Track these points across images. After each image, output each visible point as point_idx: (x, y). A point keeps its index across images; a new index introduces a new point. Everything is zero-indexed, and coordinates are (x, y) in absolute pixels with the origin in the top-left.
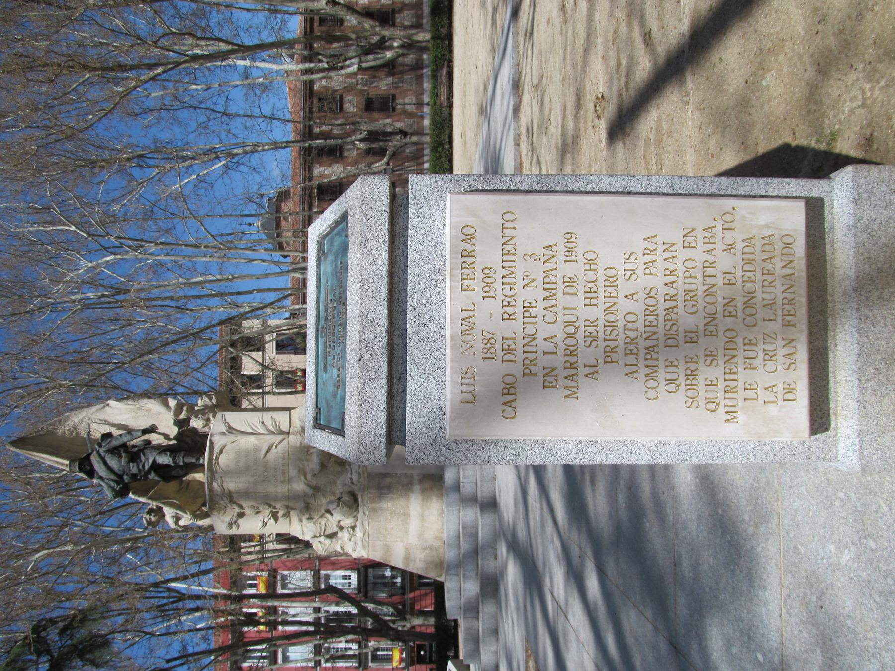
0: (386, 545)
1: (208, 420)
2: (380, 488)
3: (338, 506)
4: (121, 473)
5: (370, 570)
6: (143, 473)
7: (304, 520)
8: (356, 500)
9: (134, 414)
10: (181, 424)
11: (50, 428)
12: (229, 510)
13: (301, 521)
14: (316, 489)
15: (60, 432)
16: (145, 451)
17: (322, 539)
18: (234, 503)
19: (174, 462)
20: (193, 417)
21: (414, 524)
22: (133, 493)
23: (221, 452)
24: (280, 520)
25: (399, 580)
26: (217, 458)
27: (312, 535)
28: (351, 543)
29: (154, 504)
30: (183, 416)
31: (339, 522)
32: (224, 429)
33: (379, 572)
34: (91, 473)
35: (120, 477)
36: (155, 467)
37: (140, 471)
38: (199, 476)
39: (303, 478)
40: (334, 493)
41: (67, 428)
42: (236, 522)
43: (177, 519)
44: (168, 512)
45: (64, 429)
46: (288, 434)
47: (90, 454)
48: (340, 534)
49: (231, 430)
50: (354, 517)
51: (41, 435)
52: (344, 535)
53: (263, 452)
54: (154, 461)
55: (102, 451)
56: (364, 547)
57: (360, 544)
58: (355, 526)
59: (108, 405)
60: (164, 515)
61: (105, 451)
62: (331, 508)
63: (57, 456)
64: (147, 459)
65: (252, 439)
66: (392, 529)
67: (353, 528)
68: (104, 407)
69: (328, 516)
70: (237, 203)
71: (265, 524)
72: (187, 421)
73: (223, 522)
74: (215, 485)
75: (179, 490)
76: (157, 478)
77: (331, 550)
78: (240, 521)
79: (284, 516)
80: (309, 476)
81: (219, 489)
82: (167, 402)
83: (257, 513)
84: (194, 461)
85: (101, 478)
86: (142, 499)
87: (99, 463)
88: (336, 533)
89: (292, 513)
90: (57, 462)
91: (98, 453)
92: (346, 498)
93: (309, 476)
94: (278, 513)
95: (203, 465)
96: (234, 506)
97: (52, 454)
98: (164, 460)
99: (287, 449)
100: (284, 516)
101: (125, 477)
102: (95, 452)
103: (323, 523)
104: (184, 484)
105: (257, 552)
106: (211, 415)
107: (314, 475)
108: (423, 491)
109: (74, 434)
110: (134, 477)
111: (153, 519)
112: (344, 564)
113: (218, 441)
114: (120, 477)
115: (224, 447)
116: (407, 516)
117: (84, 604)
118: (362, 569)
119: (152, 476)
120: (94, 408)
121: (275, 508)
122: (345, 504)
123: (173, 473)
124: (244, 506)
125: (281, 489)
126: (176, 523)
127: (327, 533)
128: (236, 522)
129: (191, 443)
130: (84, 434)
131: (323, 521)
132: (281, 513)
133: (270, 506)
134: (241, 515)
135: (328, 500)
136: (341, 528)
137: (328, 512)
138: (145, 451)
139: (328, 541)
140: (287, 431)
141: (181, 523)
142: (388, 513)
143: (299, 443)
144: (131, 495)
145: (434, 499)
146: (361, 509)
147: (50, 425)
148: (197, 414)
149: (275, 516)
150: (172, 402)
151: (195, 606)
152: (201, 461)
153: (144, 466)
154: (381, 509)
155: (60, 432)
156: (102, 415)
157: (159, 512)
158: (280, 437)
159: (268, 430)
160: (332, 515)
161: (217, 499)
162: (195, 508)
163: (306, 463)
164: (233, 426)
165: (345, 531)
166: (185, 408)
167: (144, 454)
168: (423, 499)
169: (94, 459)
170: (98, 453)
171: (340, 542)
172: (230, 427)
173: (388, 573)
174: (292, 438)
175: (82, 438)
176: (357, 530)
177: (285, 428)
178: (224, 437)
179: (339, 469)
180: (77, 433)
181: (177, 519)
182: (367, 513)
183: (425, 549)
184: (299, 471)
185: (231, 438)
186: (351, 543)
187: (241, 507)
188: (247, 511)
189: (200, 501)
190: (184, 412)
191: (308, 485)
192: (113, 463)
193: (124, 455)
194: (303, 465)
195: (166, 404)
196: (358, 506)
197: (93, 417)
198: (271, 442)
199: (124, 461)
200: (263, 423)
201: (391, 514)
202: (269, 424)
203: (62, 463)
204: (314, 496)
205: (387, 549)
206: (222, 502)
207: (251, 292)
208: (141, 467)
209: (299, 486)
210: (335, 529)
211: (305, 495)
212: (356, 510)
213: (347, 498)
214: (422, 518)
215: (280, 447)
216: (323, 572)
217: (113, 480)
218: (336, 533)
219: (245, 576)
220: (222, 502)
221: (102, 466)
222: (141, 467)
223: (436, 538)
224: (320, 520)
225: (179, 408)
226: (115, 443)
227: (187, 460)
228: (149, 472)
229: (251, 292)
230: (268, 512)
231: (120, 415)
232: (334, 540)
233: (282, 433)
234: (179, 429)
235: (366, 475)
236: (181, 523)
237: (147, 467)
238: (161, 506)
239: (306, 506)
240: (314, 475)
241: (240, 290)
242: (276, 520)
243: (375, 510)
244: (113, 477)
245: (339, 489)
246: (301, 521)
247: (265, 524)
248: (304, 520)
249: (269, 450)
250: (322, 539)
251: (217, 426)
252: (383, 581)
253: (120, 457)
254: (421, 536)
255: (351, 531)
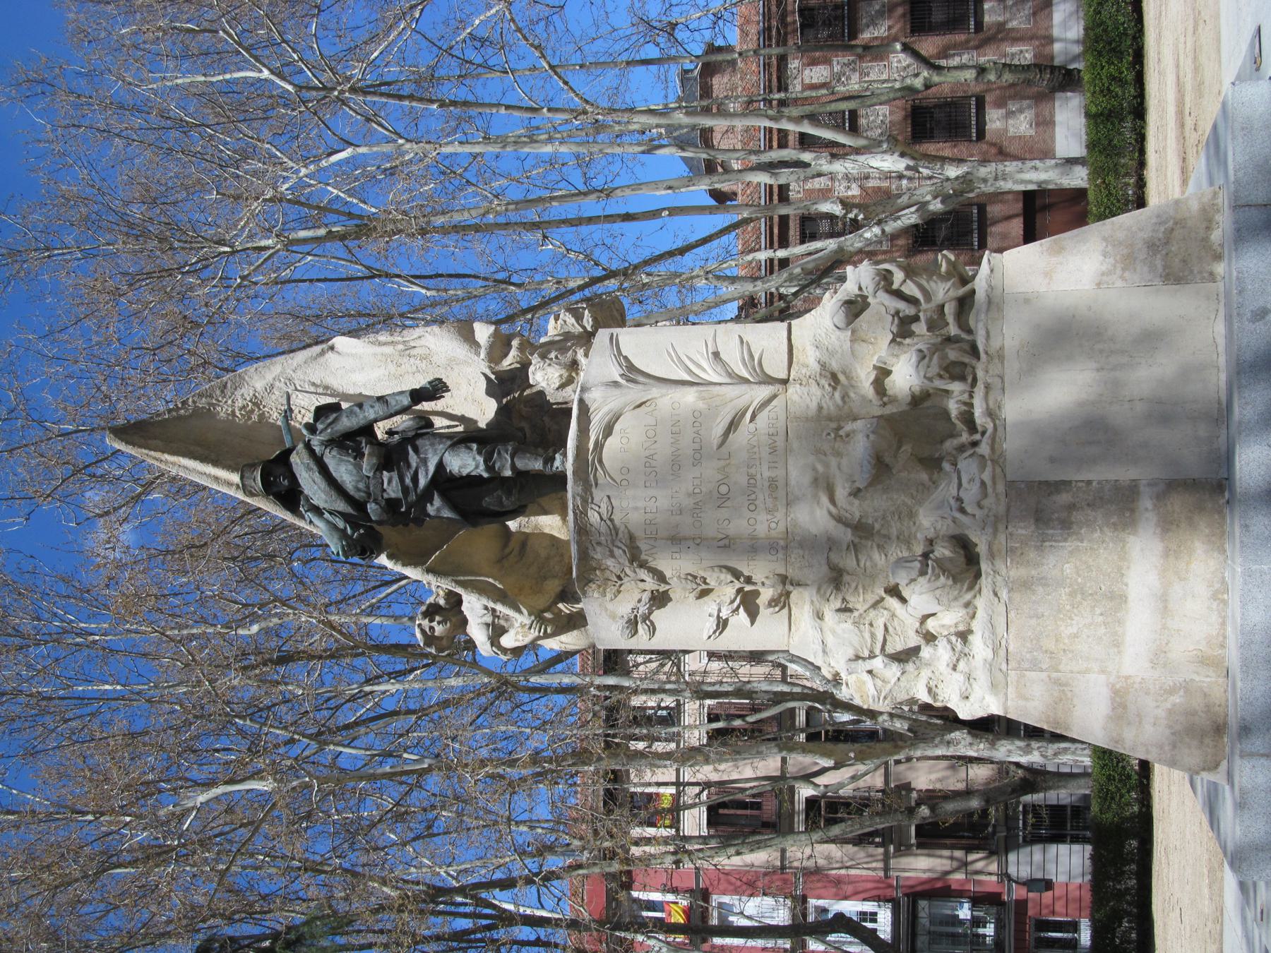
0: (1057, 682)
1: (574, 365)
2: (1041, 518)
3: (923, 573)
4: (359, 496)
5: (923, 904)
6: (412, 497)
7: (830, 616)
8: (971, 559)
9: (392, 368)
10: (505, 385)
11: (202, 403)
12: (628, 584)
13: (819, 616)
14: (863, 531)
15: (222, 411)
16: (419, 442)
17: (878, 663)
18: (643, 565)
19: (489, 468)
20: (535, 359)
21: (1139, 623)
22: (390, 557)
23: (608, 430)
24: (764, 612)
25: (989, 930)
26: (599, 446)
27: (850, 653)
28: (958, 677)
29: (437, 588)
30: (510, 361)
31: (925, 618)
32: (615, 373)
33: (945, 909)
34: (291, 497)
35: (360, 506)
36: (444, 482)
37: (405, 490)
38: (550, 524)
39: (825, 500)
40: (907, 541)
41: (240, 403)
42: (646, 618)
43: (496, 631)
44: (473, 606)
45: (233, 404)
46: (785, 382)
47: (288, 453)
48: (926, 652)
49: (632, 372)
50: (967, 605)
51: (180, 418)
52: (940, 655)
53: (719, 430)
54: (440, 466)
55: (316, 442)
56: (993, 686)
57: (982, 677)
58: (970, 632)
59: (332, 348)
60: (465, 622)
61: (322, 443)
62: (901, 579)
63: (216, 463)
64: (424, 462)
65: (689, 397)
66: (1076, 636)
67: (964, 636)
68: (323, 353)
69: (892, 602)
70: (617, 47)
71: (722, 624)
72: (519, 376)
73: (613, 617)
74: (593, 517)
75: (501, 560)
76: (447, 514)
77: (902, 696)
78: (657, 616)
79: (773, 603)
80: (841, 493)
81: (603, 529)
82: (473, 332)
83: (704, 593)
84: (538, 465)
85: (317, 511)
86: (413, 573)
87: (309, 469)
88: (916, 650)
89: (794, 596)
90: (216, 479)
91: (308, 446)
92: (943, 551)
93: (841, 493)
94: (756, 594)
95: (560, 479)
96: (643, 574)
97: (204, 459)
98: (465, 463)
99: (781, 424)
100: (773, 603)
101: (371, 507)
102: (300, 446)
103: (879, 624)
104: (514, 544)
105: (666, 841)
106: (580, 352)
107: (856, 493)
108: (1167, 525)
109: (255, 417)
110: (392, 506)
111: (439, 630)
112: (862, 886)
113: (602, 404)
114: (360, 506)
115: (617, 417)
116: (1118, 599)
117: (297, 915)
118: (904, 901)
119: (436, 506)
120: (301, 356)
121: (749, 580)
122: (943, 567)
123: (488, 502)
124: (668, 574)
125: (764, 524)
126: (494, 641)
127: (890, 649)
128: (646, 618)
129: (529, 422)
130: (275, 417)
131: (880, 619)
132: (766, 594)
133: (736, 574)
134: (660, 600)
135: (892, 559)
136: (930, 638)
137: (894, 592)
138: (419, 442)
139: (894, 670)
140: (783, 376)
141: (508, 641)
142: (1064, 592)
143: (814, 405)
144: (383, 560)
145: (1199, 547)
146: (985, 582)
147: (201, 395)
148: (544, 352)
149: (749, 603)
150: (483, 332)
151: (533, 937)
152: (557, 463)
153: (415, 479)
154: (1043, 581)
155: (222, 411)
156: (317, 374)
157: (452, 609)
158: (764, 392)
159: (731, 374)
160: (903, 600)
161: (598, 554)
162: (542, 602)
163: (833, 461)
164: (637, 363)
165: (942, 644)
166: (515, 343)
167: (416, 450)
168: (1166, 553)
169: (299, 462)
170: (308, 446)
171: (925, 673)
172: (631, 367)
173: (965, 912)
174: (794, 391)
175: (273, 425)
176: (976, 640)
177: (776, 368)
178: (616, 392)
179: (924, 476)
180: (262, 416)
181: (496, 631)
182: (1004, 594)
183: (1172, 691)
184: (815, 481)
185: (634, 393)
186: (958, 677)
187: (661, 577)
188: (677, 590)
189: (553, 586)
190: (513, 353)
191: (839, 520)
192: (343, 470)
193: (366, 451)
194: (827, 465)
195: (468, 337)
196: (978, 575)
197: (298, 378)
198: (741, 403)
199: (367, 465)
200: (716, 355)
201: (1072, 594)
202: (733, 356)
203: (222, 480)
204: (855, 548)
205: (1062, 689)
206: (610, 562)
207: (655, 214)
208: (408, 481)
209: (814, 517)
210: (913, 640)
211: (831, 544)
212: (971, 588)
213: (947, 553)
214: (1164, 604)
215: (763, 417)
216: (813, 902)
217: (344, 516)
218: (916, 650)
219: (637, 901)
220: (610, 562)
221: (317, 476)
222: (408, 481)
223: (1204, 661)
224: (872, 613)
225: (500, 346)
226: (346, 423)
227: (520, 464)
228: (426, 496)
229: (655, 214)
230: (730, 591)
231: (362, 368)
232: (910, 667)
233: (768, 380)
234: (499, 402)
235: (1001, 488)
236: (508, 641)
237: (422, 482)
238: (459, 590)
239: (834, 567)
240: (856, 493)
241: (643, 68)
242: (753, 614)
243: (1026, 585)
244: (341, 506)
245: (928, 521)
246: (819, 616)
247: (722, 624)
248: (830, 616)
249: (733, 425)
250: (878, 663)
251: (598, 365)
252: (951, 929)
253: (359, 455)
254: (1159, 657)
255: (959, 645)
